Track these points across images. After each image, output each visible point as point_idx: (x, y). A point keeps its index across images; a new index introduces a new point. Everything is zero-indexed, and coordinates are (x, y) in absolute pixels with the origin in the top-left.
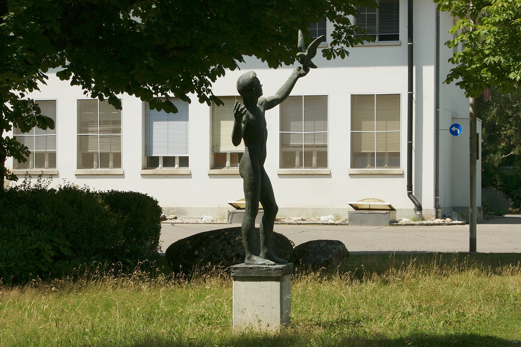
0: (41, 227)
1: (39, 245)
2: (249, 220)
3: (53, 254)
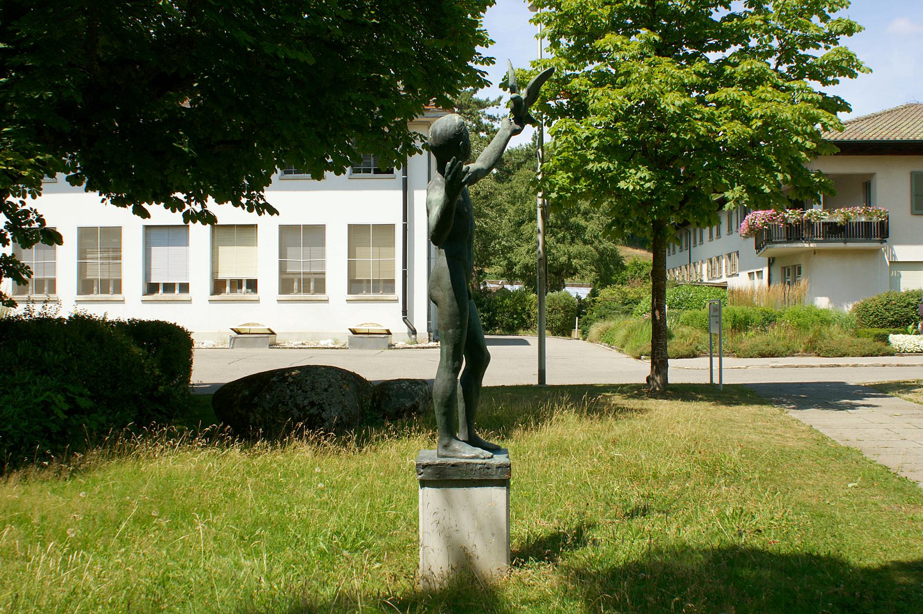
0: (49, 371)
1: (48, 397)
2: (449, 380)
3: (66, 407)
